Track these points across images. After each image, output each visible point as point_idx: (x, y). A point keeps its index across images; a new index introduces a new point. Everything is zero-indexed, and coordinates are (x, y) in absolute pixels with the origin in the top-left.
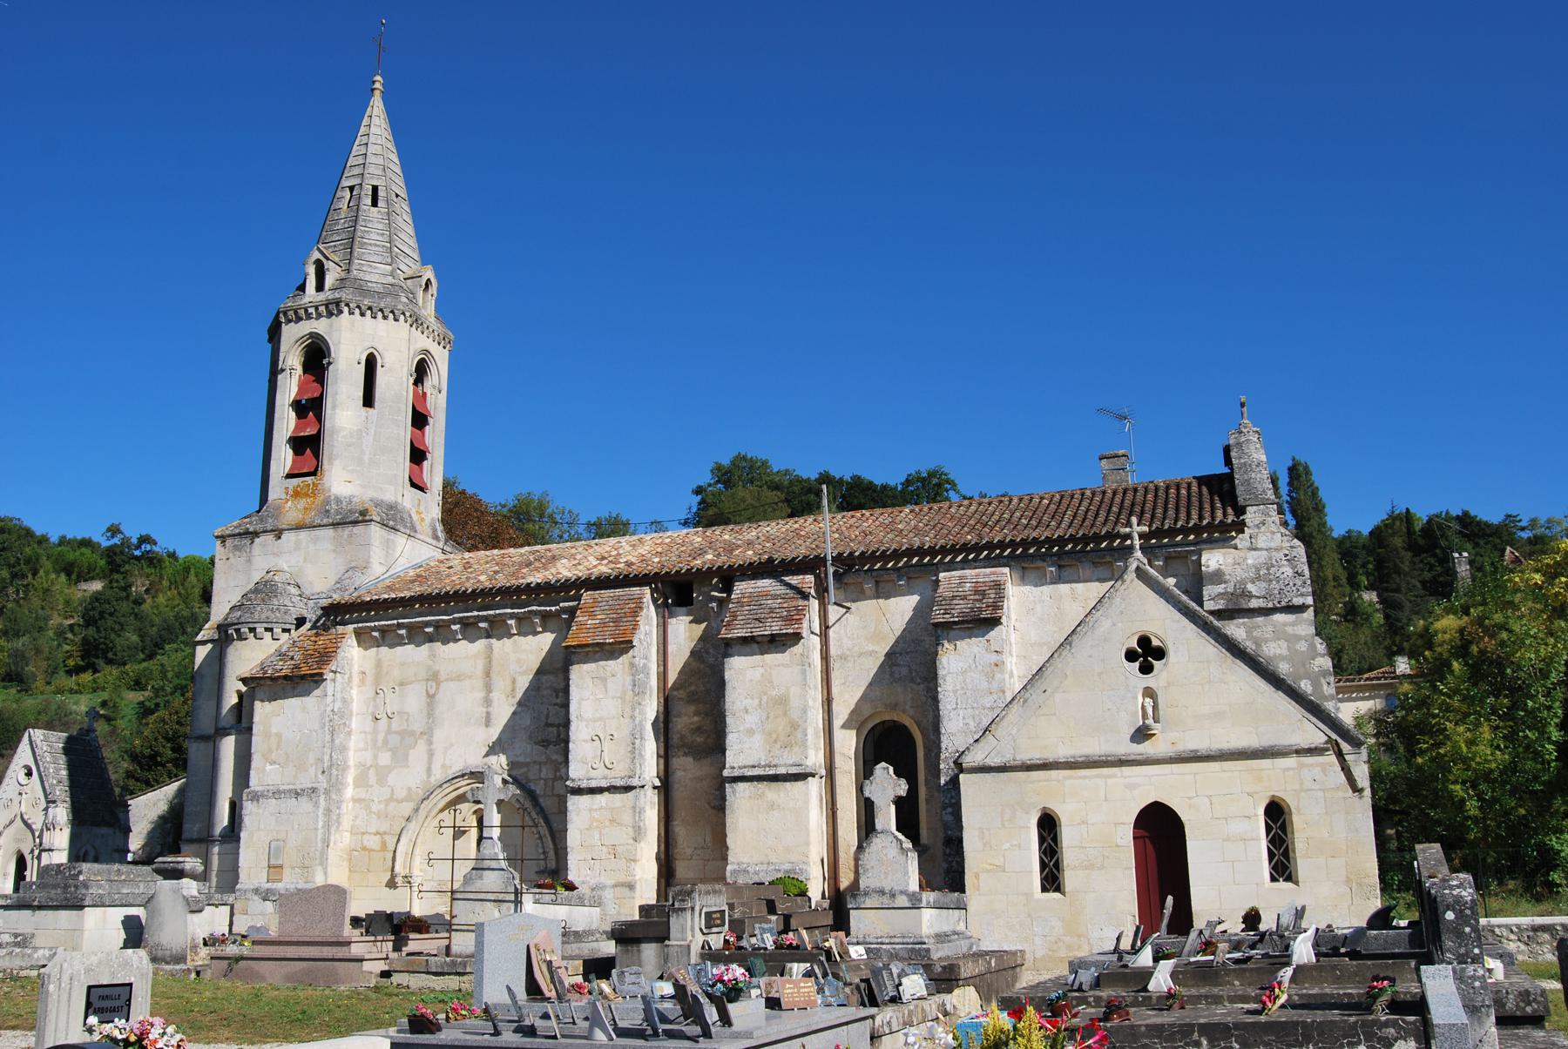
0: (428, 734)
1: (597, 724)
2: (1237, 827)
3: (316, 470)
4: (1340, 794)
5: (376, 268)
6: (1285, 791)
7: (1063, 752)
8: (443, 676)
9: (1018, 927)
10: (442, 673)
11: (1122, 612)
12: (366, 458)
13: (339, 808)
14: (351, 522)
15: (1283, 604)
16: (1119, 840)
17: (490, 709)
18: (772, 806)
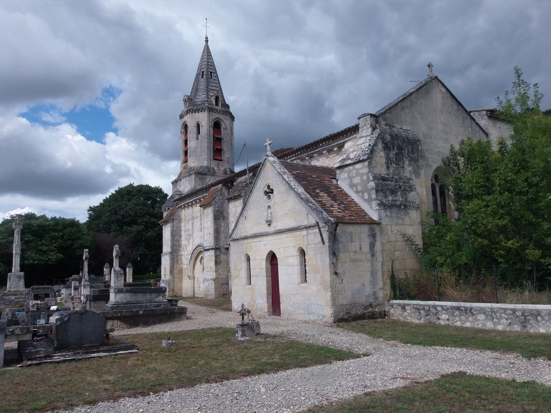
0: (192, 235)
3: (187, 160)
4: (319, 246)
5: (201, 97)
7: (251, 232)
12: (198, 155)
15: (357, 160)
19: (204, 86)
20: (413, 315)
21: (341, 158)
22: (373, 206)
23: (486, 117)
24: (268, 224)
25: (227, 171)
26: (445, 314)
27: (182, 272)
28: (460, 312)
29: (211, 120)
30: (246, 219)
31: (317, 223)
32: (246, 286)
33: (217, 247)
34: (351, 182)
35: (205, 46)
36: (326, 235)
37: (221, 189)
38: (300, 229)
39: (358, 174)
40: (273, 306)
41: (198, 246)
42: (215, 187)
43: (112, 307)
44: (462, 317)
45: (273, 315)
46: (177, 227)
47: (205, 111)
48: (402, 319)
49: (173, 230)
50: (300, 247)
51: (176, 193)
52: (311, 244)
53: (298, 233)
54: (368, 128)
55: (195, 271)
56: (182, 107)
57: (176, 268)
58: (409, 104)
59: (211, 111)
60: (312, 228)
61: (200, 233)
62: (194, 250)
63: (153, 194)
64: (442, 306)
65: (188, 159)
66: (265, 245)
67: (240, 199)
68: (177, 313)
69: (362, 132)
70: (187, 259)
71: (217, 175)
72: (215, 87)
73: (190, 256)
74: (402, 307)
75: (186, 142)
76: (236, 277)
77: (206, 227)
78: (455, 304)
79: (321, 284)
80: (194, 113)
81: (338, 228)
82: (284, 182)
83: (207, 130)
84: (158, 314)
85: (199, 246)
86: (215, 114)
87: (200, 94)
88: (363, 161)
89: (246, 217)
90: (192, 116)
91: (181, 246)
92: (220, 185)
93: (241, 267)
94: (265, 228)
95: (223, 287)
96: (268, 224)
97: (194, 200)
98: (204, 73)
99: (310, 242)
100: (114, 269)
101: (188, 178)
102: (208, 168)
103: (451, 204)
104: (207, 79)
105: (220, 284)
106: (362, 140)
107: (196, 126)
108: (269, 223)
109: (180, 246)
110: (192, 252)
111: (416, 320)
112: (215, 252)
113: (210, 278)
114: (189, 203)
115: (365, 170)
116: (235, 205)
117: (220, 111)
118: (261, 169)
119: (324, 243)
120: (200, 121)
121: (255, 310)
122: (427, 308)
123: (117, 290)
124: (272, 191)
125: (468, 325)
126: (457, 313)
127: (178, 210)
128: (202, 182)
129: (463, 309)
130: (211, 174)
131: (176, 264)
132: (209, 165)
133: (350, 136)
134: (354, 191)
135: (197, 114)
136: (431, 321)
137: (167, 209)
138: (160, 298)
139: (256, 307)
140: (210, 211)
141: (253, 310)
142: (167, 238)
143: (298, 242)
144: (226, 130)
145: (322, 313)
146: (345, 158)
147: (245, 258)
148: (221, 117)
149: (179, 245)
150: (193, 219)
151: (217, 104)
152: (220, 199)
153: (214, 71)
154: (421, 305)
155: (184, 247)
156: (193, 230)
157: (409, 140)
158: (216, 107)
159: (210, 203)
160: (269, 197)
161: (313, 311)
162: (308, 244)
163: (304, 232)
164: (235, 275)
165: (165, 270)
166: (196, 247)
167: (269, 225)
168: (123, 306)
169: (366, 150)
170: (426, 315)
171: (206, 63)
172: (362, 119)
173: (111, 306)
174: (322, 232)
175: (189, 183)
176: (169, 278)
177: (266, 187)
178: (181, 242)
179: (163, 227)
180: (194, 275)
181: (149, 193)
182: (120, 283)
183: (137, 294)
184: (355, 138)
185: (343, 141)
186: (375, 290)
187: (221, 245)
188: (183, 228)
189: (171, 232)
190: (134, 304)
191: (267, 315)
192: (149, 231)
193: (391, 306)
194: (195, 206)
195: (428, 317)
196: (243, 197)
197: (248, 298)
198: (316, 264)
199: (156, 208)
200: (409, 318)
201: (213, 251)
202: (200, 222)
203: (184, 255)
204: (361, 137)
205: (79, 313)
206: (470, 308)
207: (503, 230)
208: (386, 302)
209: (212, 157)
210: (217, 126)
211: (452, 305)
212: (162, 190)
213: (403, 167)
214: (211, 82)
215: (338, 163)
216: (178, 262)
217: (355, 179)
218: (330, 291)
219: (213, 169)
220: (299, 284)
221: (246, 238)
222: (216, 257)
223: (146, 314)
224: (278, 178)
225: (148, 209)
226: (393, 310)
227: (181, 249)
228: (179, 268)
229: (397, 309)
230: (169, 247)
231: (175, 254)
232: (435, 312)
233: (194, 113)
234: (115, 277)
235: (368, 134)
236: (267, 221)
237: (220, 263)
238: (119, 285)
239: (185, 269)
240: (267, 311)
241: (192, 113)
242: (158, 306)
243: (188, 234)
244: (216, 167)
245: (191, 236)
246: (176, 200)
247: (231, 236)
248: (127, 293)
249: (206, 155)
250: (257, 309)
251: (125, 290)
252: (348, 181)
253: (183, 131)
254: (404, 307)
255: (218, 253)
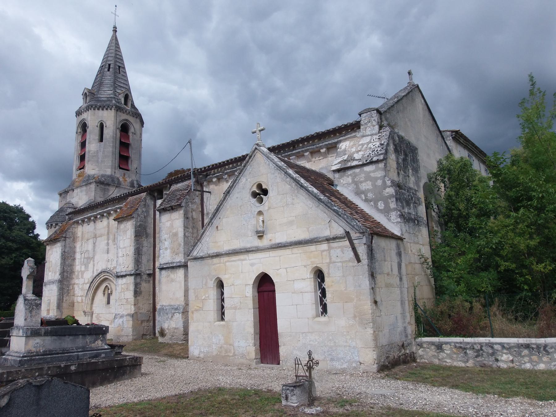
0: (93, 258)
1: (124, 249)
2: (299, 285)
3: (84, 167)
4: (351, 264)
5: (106, 92)
6: (322, 263)
7: (226, 248)
8: (97, 235)
9: (207, 339)
10: (97, 235)
11: (250, 173)
12: (100, 160)
13: (68, 287)
14: (90, 183)
15: (368, 161)
16: (247, 294)
17: (109, 247)
18: (172, 281)
19: (110, 81)
20: (455, 356)
21: (340, 159)
22: (392, 218)
23: (451, 138)
24: (258, 236)
25: (134, 184)
26: (506, 355)
27: (73, 306)
28: (530, 350)
29: (118, 121)
30: (218, 230)
31: (348, 233)
32: (215, 322)
33: (138, 272)
34: (358, 187)
35: (113, 37)
36: (362, 250)
37: (145, 198)
38: (315, 242)
39: (368, 178)
40: (261, 350)
41: (101, 273)
42: (135, 197)
43: (20, 361)
44: (533, 357)
45: (262, 362)
46: (70, 247)
47: (111, 109)
48: (436, 361)
49: (64, 252)
50: (218, 277)
51: (68, 205)
52: (336, 262)
53: (312, 248)
54: (374, 126)
55: (94, 305)
56: (80, 102)
57: (66, 301)
58: (402, 107)
59: (119, 110)
60: (338, 241)
61: (106, 255)
62: (95, 277)
63: (11, 213)
64: (502, 345)
65: (86, 165)
66: (252, 265)
67: (180, 210)
68: (128, 366)
69: (365, 130)
70: (82, 289)
71: (122, 187)
72: (124, 84)
73: (88, 285)
74: (436, 346)
75: (83, 145)
76: (196, 310)
77: (121, 246)
78: (521, 341)
79: (355, 317)
80: (96, 110)
81: (373, 241)
82: (288, 179)
83: (113, 132)
84: (100, 370)
85: (104, 272)
86: (124, 114)
87: (105, 89)
88: (377, 162)
89: (217, 227)
90: (95, 113)
91: (74, 272)
92: (144, 195)
93: (207, 296)
94: (257, 243)
95: (143, 324)
96: (258, 236)
97: (99, 214)
98: (111, 66)
99: (334, 259)
100: (24, 297)
101: (84, 188)
102: (112, 177)
103: (434, 226)
104: (115, 72)
105: (139, 321)
106: (368, 139)
107: (99, 126)
108: (260, 235)
109: (72, 272)
110: (91, 280)
111: (459, 363)
112: (135, 279)
113: (125, 313)
114: (91, 216)
115: (380, 174)
116: (170, 218)
117: (129, 112)
118: (248, 162)
119: (359, 260)
120: (105, 120)
121: (232, 356)
122: (477, 347)
123: (30, 332)
124: (265, 192)
125: (542, 366)
126: (526, 352)
127: (73, 226)
128: (104, 194)
129: (534, 346)
130: (116, 185)
131: (66, 296)
132: (113, 174)
133: (345, 136)
134: (362, 200)
135: (101, 111)
136: (484, 364)
137: (54, 225)
138: (99, 343)
139: (234, 353)
140: (129, 227)
141: (228, 356)
142: (54, 262)
143: (313, 260)
144: (135, 135)
145: (357, 358)
146: (347, 158)
147: (214, 283)
148: (131, 119)
149: (71, 270)
150: (95, 237)
151: (126, 103)
152: (143, 211)
153: (122, 66)
154: (468, 343)
155: (78, 275)
156: (94, 251)
157: (410, 146)
158: (125, 106)
159: (131, 215)
160: (261, 201)
161: (341, 355)
162: (331, 262)
163: (324, 246)
164: (196, 307)
165: (49, 304)
166: (99, 274)
167: (260, 237)
168: (40, 359)
169: (379, 149)
170: (477, 357)
171: (113, 55)
172: (365, 115)
173: (19, 359)
174: (356, 246)
175: (86, 194)
176: (55, 314)
177: (255, 187)
178: (74, 267)
179: (48, 248)
180: (92, 310)
181: (6, 212)
182: (34, 319)
183: (63, 338)
184: (355, 137)
185: (336, 140)
186: (405, 325)
187: (143, 269)
188: (78, 250)
189: (62, 253)
190: (58, 354)
191: (254, 364)
192: (4, 258)
193: (418, 345)
194: (99, 221)
195: (479, 359)
196: (183, 208)
197: (220, 340)
198: (346, 290)
199: (14, 231)
200: (448, 361)
201: (133, 277)
202: (106, 242)
203: (77, 284)
204: (363, 136)
205: (35, 386)
206: (543, 345)
207: (531, 252)
208: (413, 340)
209: (117, 165)
210: (124, 128)
211: (517, 342)
212: (23, 209)
213: (408, 176)
214: (119, 78)
215: (336, 164)
216: (68, 293)
217: (364, 184)
218: (372, 326)
219: (118, 179)
220: (314, 318)
221: (218, 255)
222: (137, 285)
223: (81, 370)
224: (276, 174)
225: (4, 230)
226: (422, 351)
227: (74, 276)
228: (70, 301)
229: (428, 350)
230: (58, 274)
231: (65, 283)
232: (491, 351)
233: (96, 110)
234: (26, 309)
235: (374, 132)
236: (257, 232)
237: (141, 293)
238: (32, 324)
239: (78, 302)
240: (254, 357)
241: (94, 109)
242: (96, 356)
243: (86, 256)
244: (121, 177)
245: (90, 259)
246: (69, 214)
247: (190, 253)
248: (47, 336)
249: (110, 162)
250: (234, 355)
251: (43, 331)
252: (351, 188)
253: (79, 130)
254: (439, 347)
255: (138, 280)
